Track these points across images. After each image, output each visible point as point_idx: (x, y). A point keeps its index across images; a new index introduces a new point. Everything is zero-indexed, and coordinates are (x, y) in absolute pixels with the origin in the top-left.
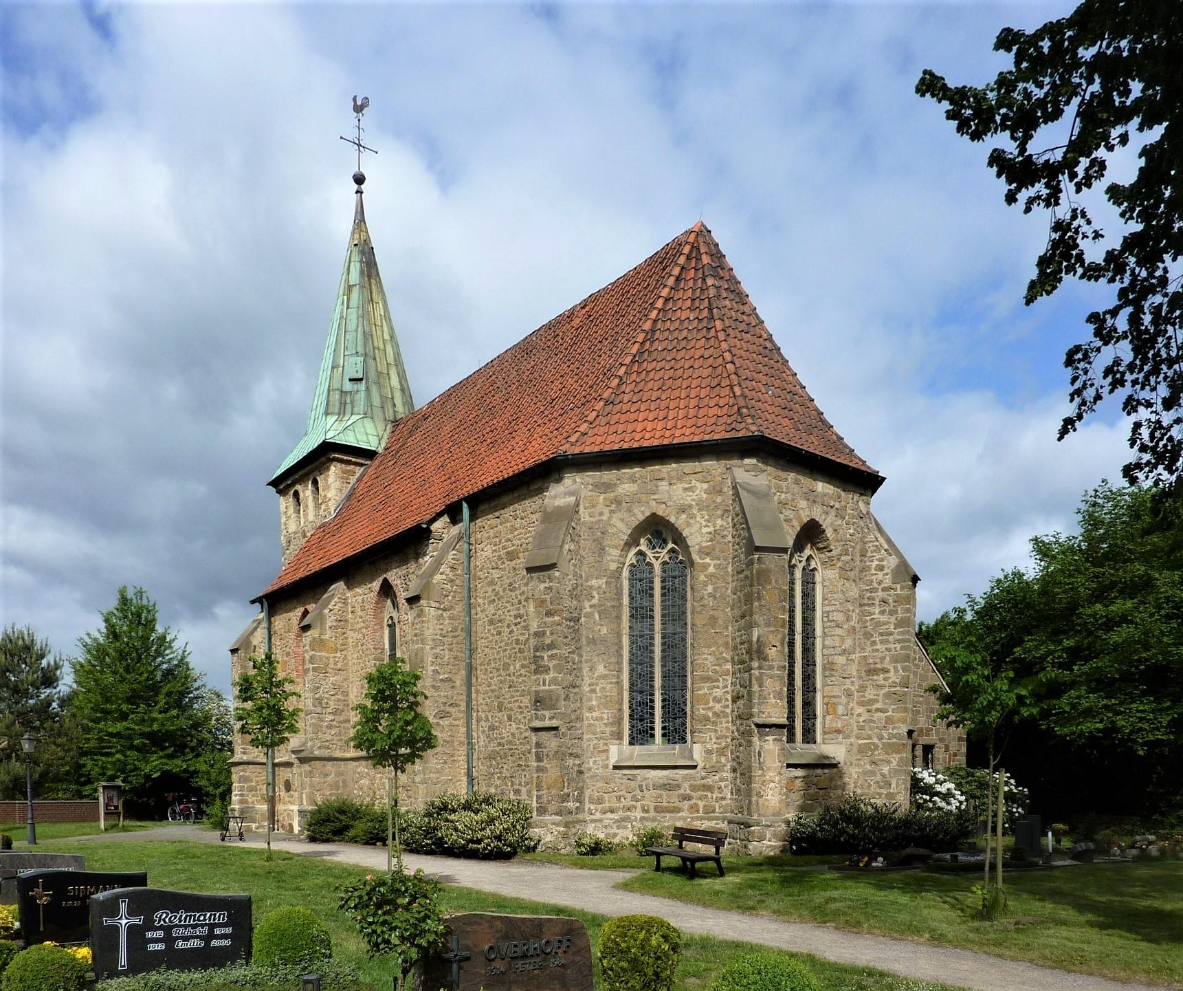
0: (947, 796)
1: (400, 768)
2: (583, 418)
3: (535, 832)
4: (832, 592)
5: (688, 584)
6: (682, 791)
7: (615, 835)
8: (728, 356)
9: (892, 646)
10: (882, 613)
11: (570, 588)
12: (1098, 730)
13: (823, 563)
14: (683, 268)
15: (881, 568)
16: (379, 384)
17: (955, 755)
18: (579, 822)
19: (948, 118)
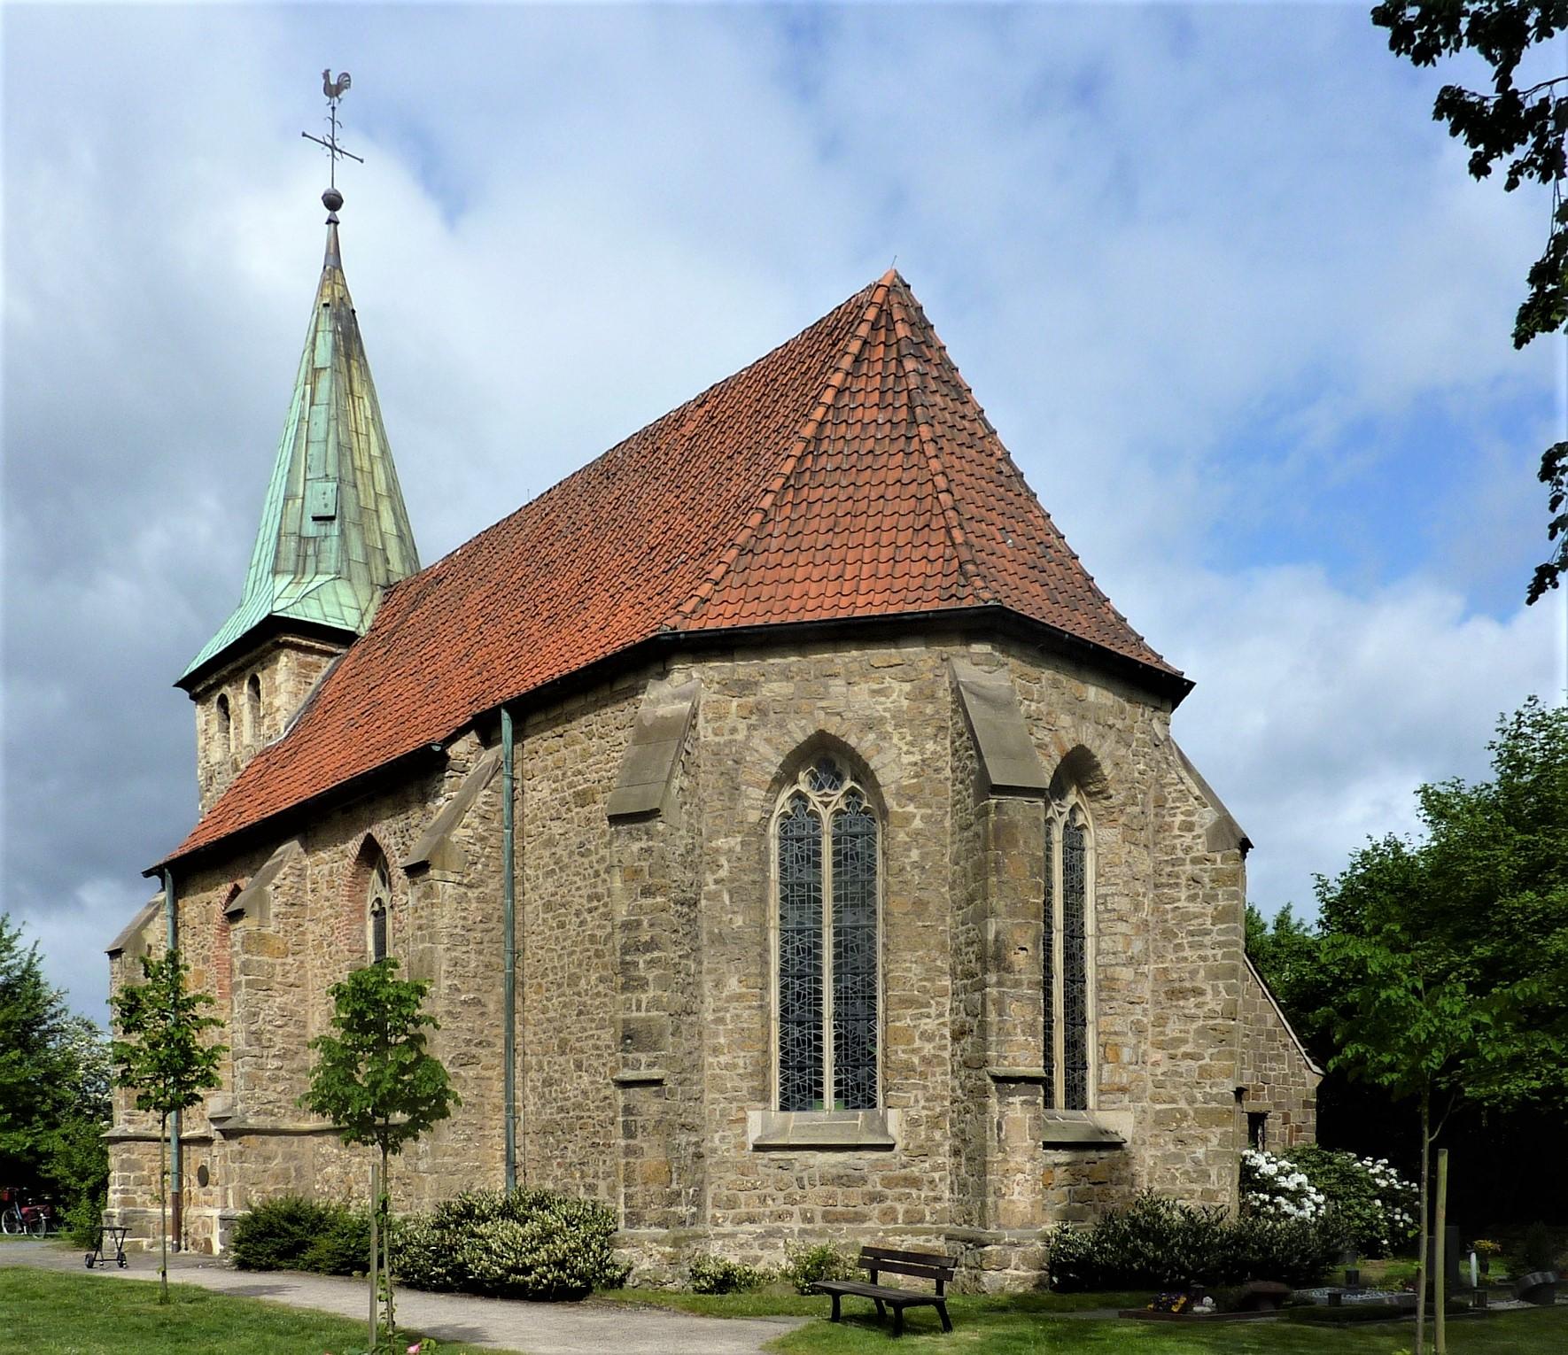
0: (1296, 1196)
1: (390, 1147)
2: (703, 576)
3: (622, 1255)
4: (1111, 865)
5: (879, 847)
6: (869, 1188)
7: (757, 1260)
8: (941, 482)
9: (1210, 952)
10: (1192, 898)
11: (682, 850)
12: (1534, 1091)
13: (1097, 818)
14: (865, 343)
15: (1189, 827)
16: (360, 525)
17: (1299, 1129)
18: (696, 1237)
19: (1376, 22)
